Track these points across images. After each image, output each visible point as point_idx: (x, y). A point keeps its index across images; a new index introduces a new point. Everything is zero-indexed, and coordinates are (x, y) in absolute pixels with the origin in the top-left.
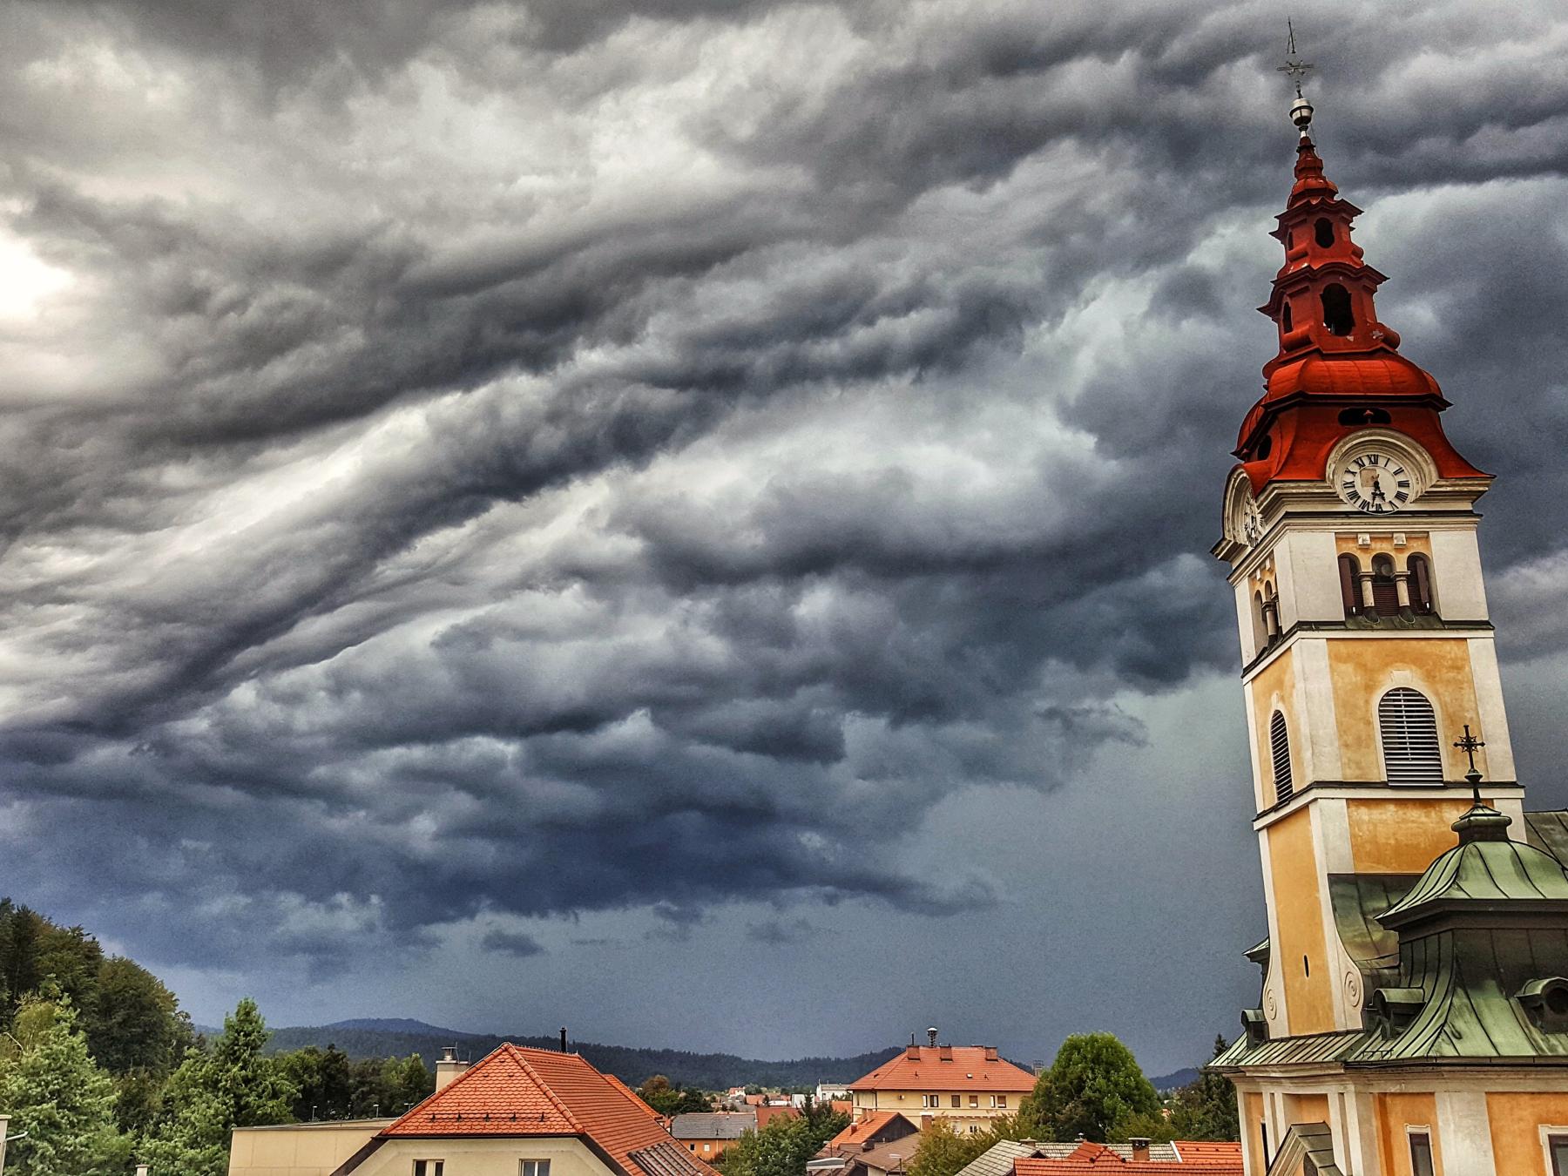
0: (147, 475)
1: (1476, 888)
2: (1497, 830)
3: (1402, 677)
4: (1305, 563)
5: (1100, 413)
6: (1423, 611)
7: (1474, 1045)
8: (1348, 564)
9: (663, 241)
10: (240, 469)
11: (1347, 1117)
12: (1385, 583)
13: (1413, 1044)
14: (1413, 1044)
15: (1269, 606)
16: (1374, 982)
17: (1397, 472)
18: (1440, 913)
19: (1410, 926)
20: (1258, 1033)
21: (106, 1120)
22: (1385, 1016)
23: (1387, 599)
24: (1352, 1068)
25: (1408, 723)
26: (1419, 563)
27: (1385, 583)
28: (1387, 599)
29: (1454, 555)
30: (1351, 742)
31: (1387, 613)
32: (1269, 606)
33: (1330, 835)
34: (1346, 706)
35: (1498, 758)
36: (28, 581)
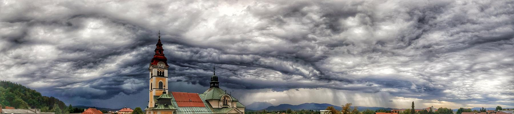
0: (59, 65)
1: (163, 97)
2: (165, 93)
3: (161, 81)
4: (155, 71)
5: (380, 29)
6: (163, 76)
7: (160, 108)
8: (158, 72)
9: (78, 48)
10: (119, 57)
11: (152, 113)
12: (161, 73)
13: (157, 108)
14: (157, 108)
15: (152, 74)
16: (155, 104)
17: (163, 65)
18: (160, 99)
19: (158, 99)
20: (148, 107)
21: (467, 73)
22: (156, 106)
23: (160, 75)
24: (153, 110)
25: (161, 84)
26: (163, 72)
27: (161, 73)
28: (160, 75)
29: (166, 72)
30: (156, 85)
31: (160, 76)
32: (152, 74)
33: (154, 93)
34: (156, 83)
35: (167, 87)
36: (511, 15)
